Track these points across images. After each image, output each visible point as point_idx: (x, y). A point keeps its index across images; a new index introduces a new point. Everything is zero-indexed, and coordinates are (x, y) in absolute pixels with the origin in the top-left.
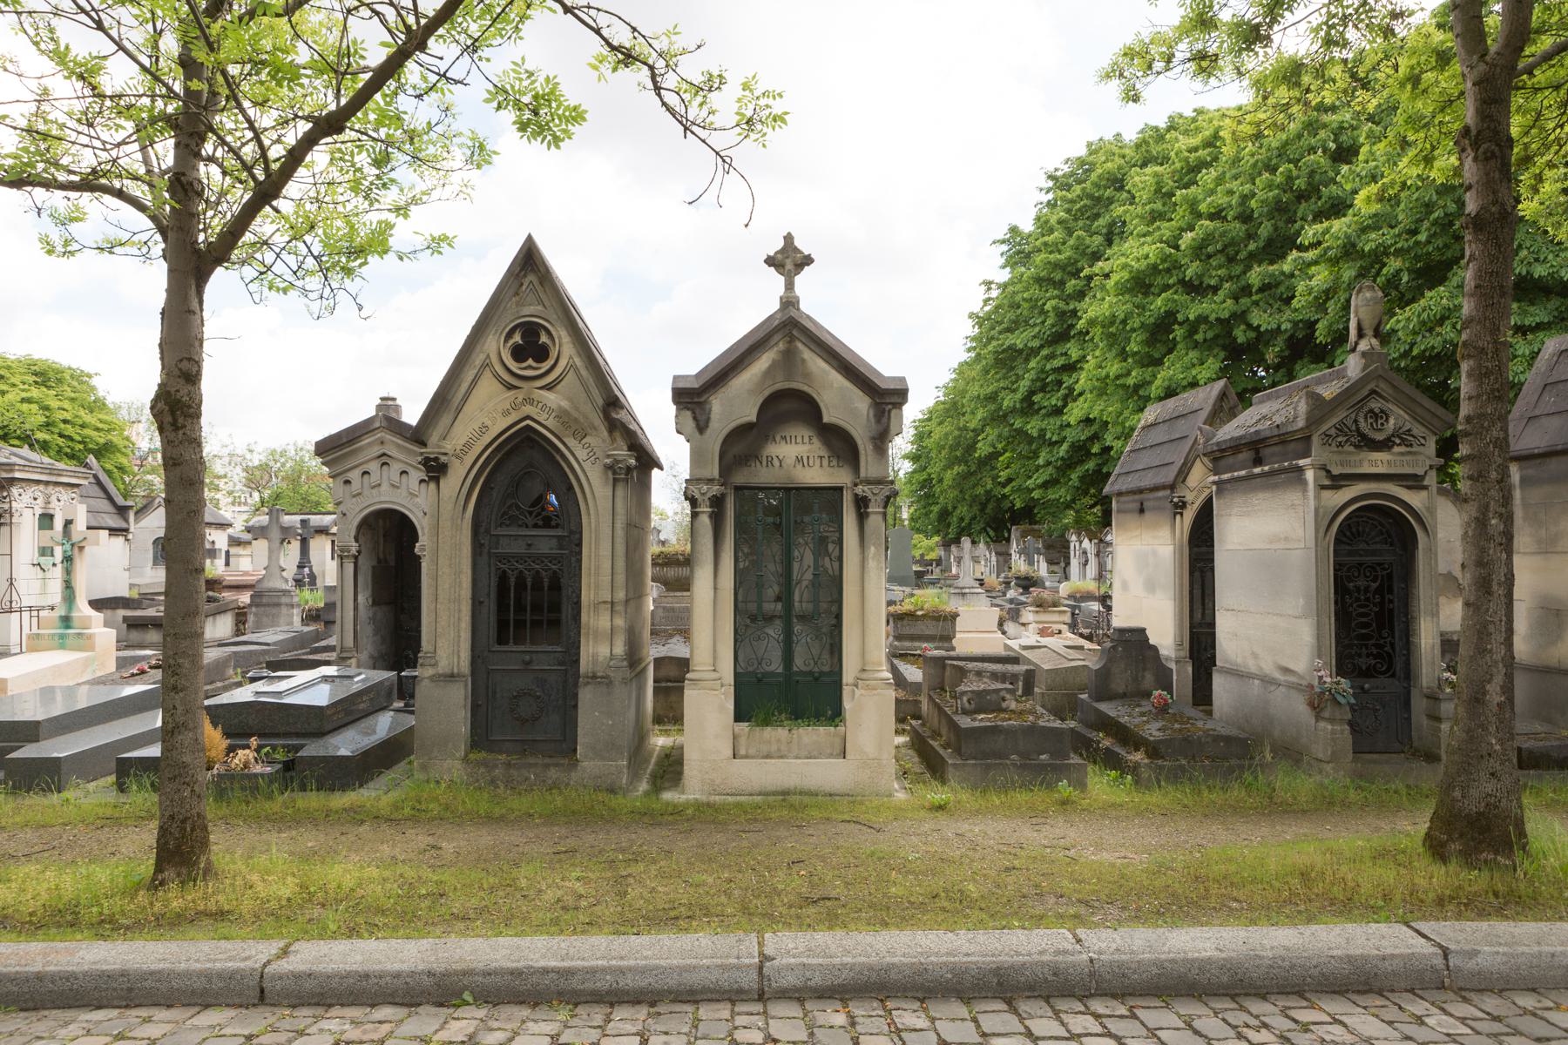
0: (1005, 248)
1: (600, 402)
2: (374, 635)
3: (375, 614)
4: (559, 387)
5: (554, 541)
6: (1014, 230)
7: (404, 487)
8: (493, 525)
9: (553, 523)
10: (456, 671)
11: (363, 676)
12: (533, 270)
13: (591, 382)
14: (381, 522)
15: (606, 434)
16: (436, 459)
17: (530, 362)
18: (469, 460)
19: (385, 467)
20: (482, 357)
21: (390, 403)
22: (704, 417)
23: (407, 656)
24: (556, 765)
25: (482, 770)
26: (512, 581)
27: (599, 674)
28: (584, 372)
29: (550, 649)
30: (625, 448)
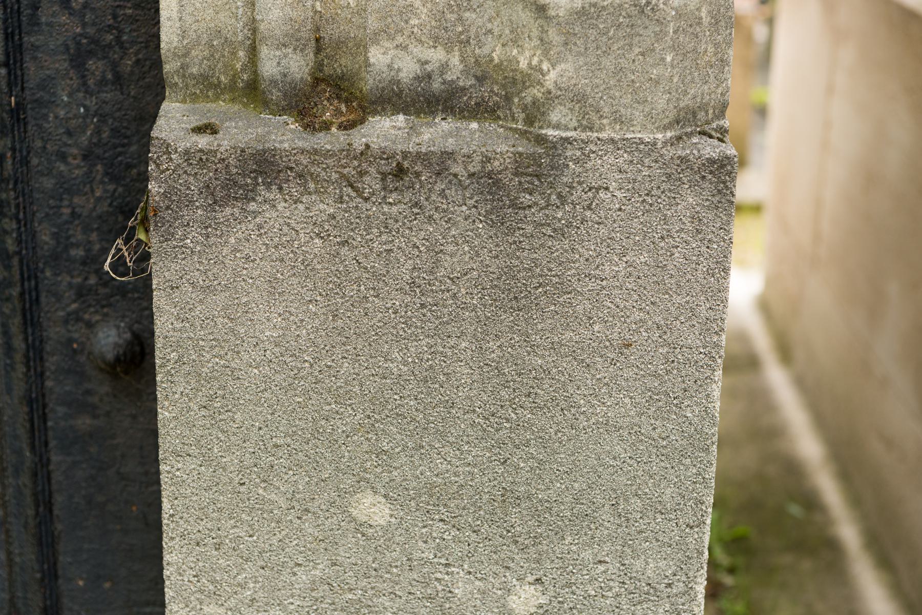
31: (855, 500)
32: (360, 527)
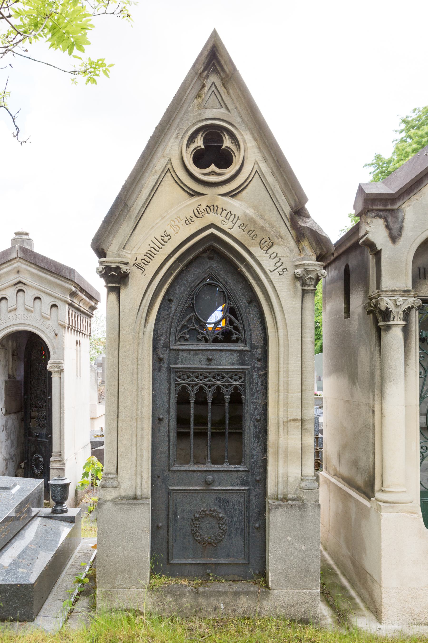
0: (372, 169)
1: (287, 210)
2: (7, 440)
3: (7, 422)
4: (243, 194)
5: (235, 357)
6: (378, 157)
7: (37, 311)
8: (172, 339)
9: (234, 337)
10: (139, 493)
11: (18, 487)
12: (215, 71)
13: (277, 188)
14: (10, 343)
15: (292, 243)
16: (118, 268)
17: (213, 167)
18: (151, 270)
19: (20, 294)
20: (164, 161)
21: (24, 237)
22: (397, 226)
23: (36, 460)
24: (247, 593)
25: (169, 599)
26: (192, 398)
27: (290, 496)
28: (270, 179)
29: (232, 468)
30: (314, 257)
31: (339, 568)
32: (288, 540)
